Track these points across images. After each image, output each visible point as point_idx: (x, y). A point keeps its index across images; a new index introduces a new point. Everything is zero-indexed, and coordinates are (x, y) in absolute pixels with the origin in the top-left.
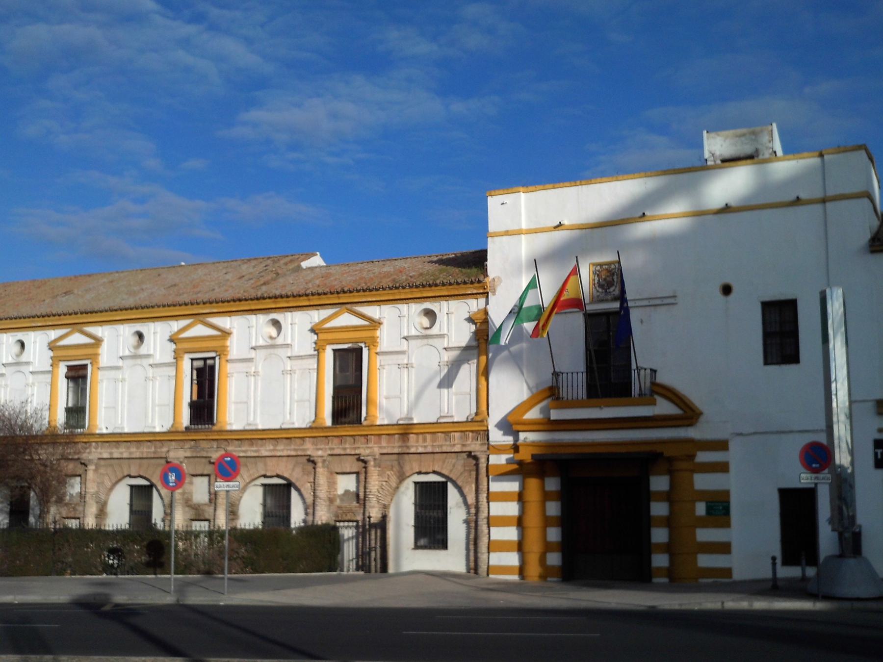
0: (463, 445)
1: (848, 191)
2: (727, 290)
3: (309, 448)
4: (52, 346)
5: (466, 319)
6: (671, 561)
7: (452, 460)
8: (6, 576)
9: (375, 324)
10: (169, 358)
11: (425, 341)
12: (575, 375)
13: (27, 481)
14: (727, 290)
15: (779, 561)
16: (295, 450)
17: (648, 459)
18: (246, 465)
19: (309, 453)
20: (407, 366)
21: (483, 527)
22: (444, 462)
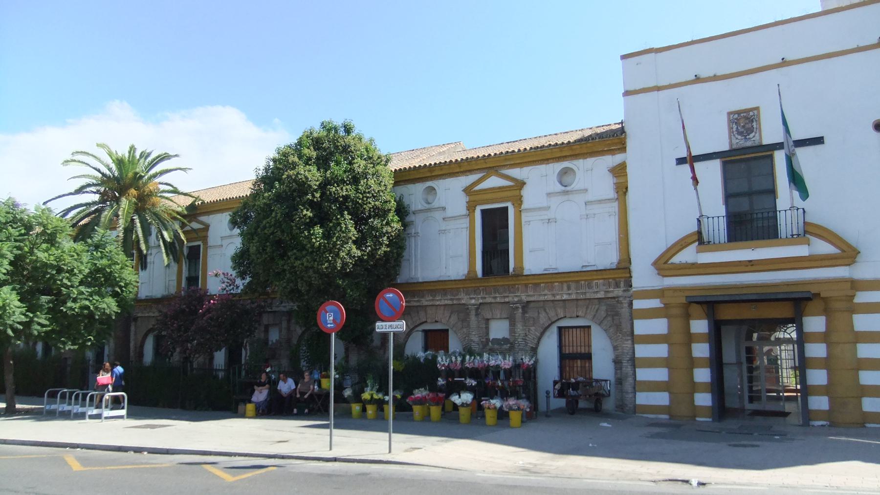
0: (606, 292)
3: (464, 299)
4: (468, 190)
8: (601, 136)
9: (521, 184)
10: (463, 210)
11: (565, 198)
13: (35, 344)
15: (551, 394)
16: (451, 299)
17: (797, 303)
19: (463, 302)
21: (628, 369)
22: (587, 308)
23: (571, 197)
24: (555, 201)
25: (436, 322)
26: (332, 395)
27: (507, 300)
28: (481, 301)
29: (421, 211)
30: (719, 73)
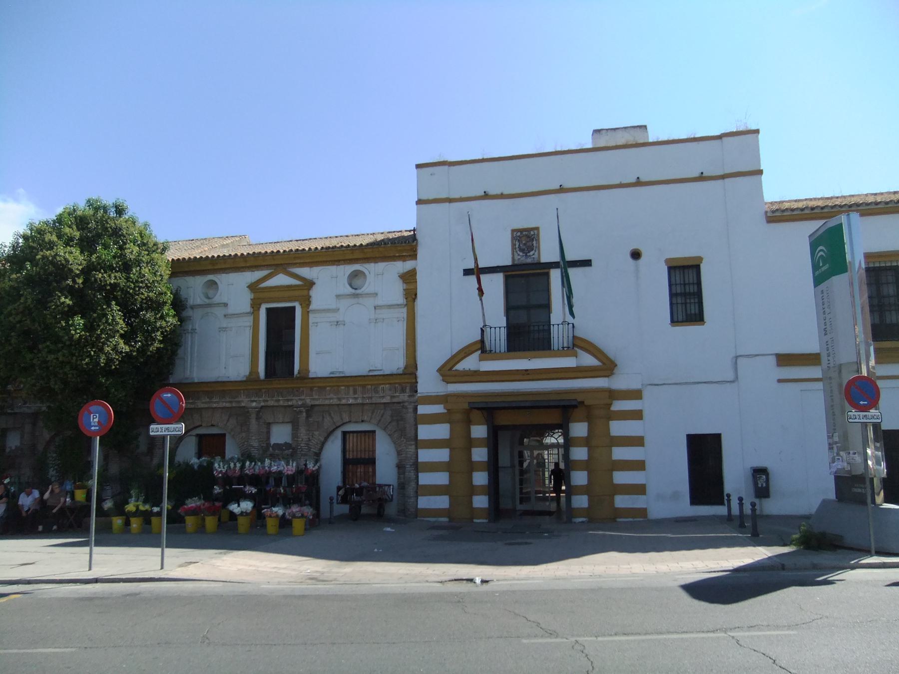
0: (392, 397)
2: (636, 255)
3: (244, 401)
4: (253, 287)
6: (469, 432)
10: (248, 309)
12: (498, 329)
14: (636, 255)
15: (335, 501)
16: (231, 402)
17: (565, 409)
19: (243, 405)
22: (372, 413)
23: (361, 300)
24: (344, 304)
27: (290, 403)
28: (263, 404)
29: (200, 306)
30: (505, 192)
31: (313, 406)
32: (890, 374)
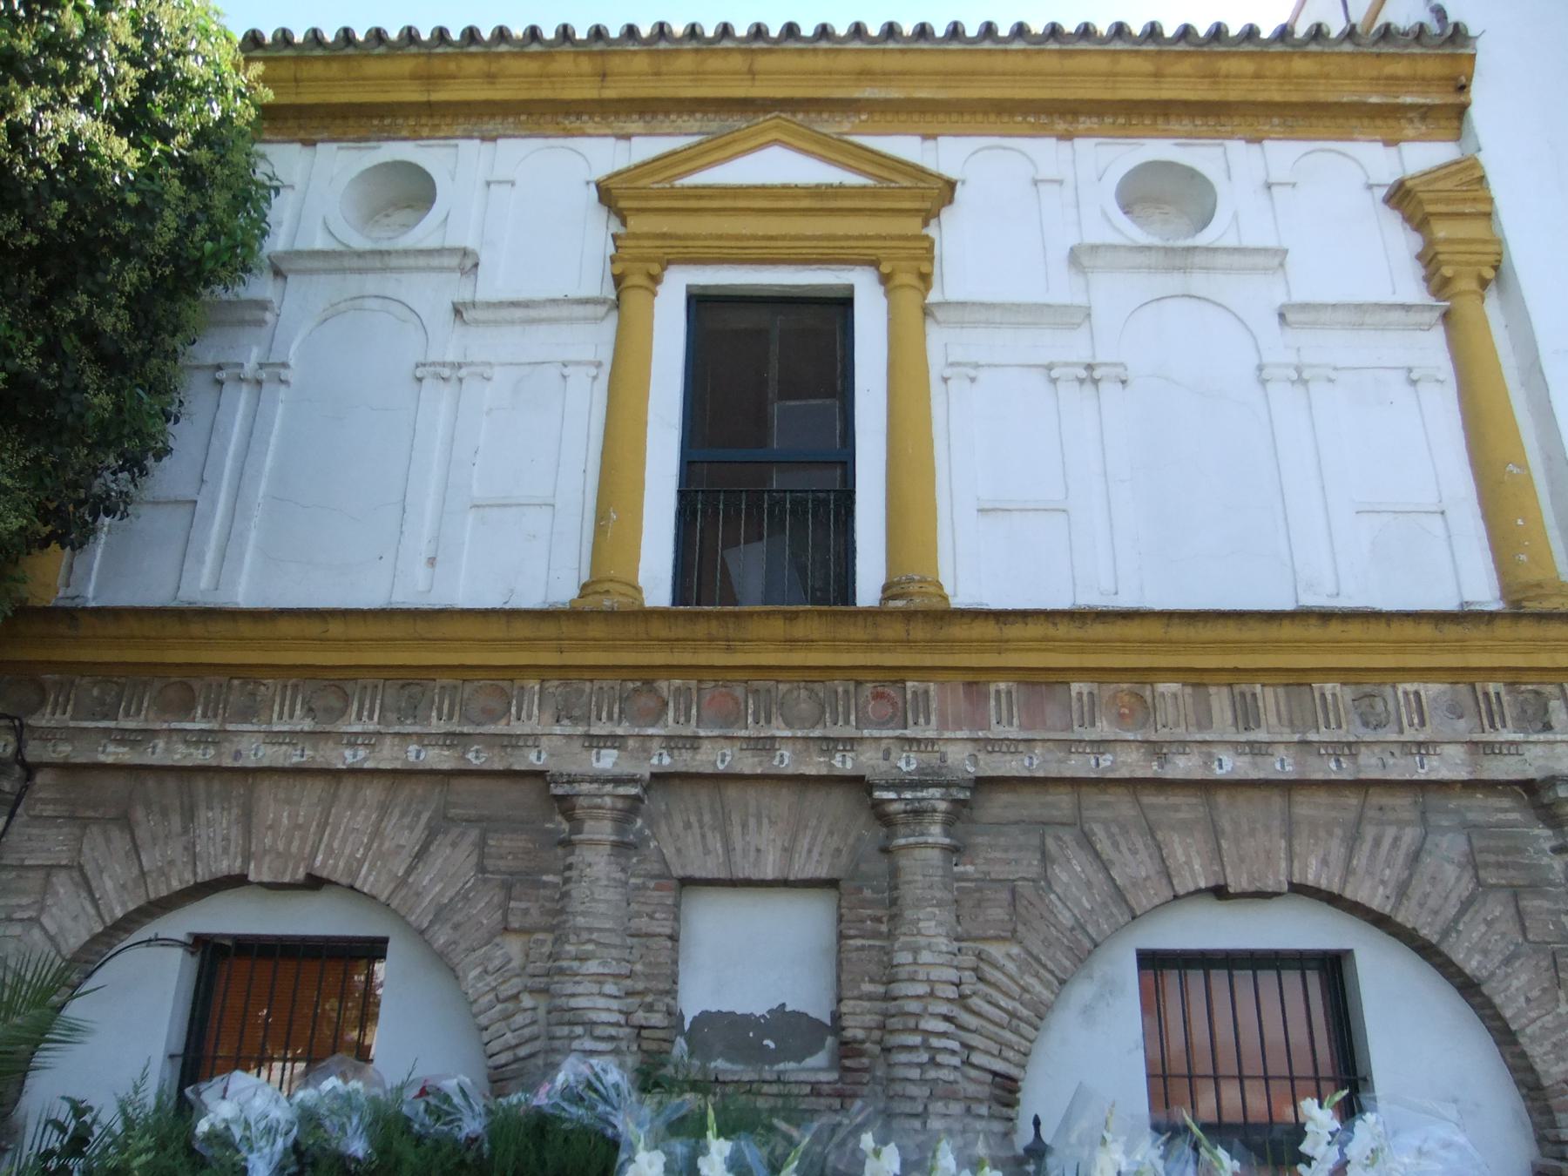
1: (1242, 1037)
3: (545, 740)
5: (91, 1032)
7: (1396, 830)
10: (594, 281)
11: (1174, 282)
16: (453, 740)
18: (125, 822)
19: (532, 759)
20: (1090, 375)
22: (1353, 841)
23: (1198, 282)
24: (1112, 294)
25: (314, 883)
26: (737, 608)
27: (844, 764)
28: (664, 761)
29: (336, 261)
31: (984, 784)
32: (1316, 1035)
